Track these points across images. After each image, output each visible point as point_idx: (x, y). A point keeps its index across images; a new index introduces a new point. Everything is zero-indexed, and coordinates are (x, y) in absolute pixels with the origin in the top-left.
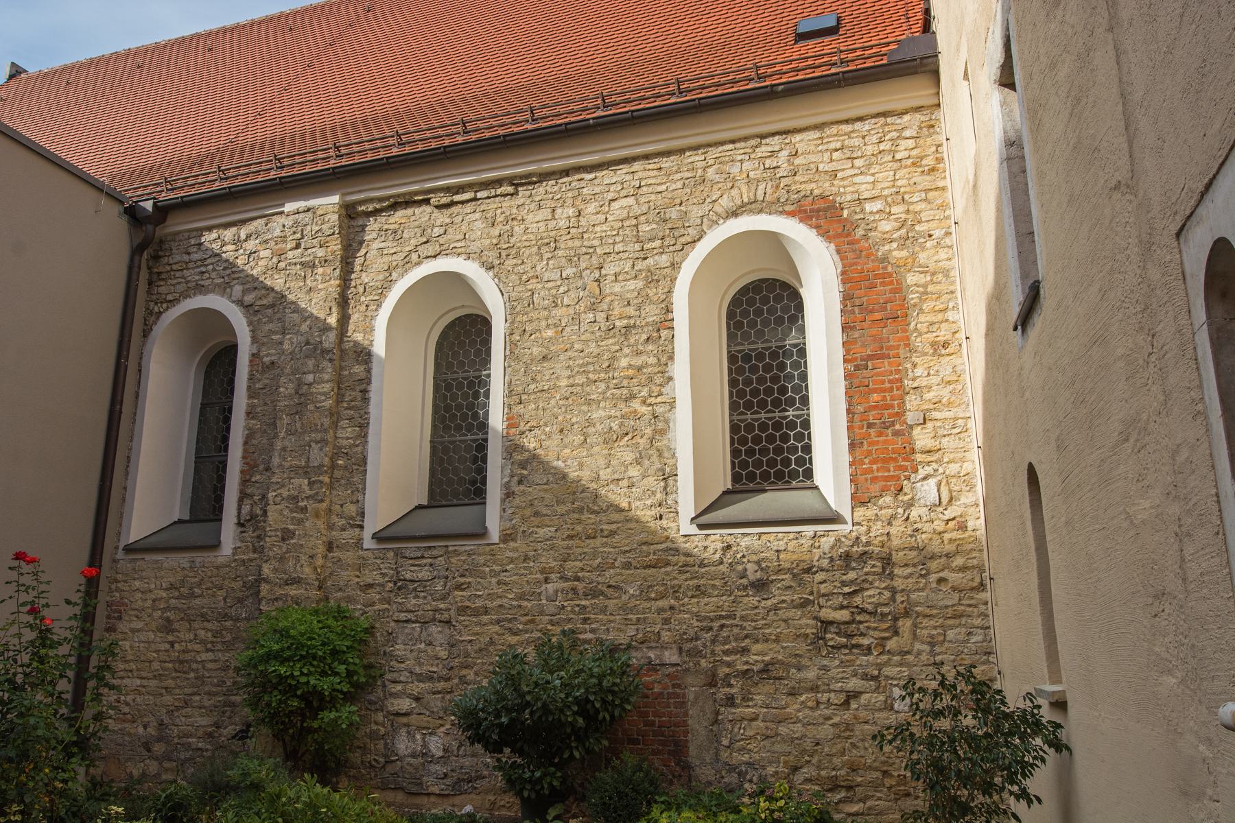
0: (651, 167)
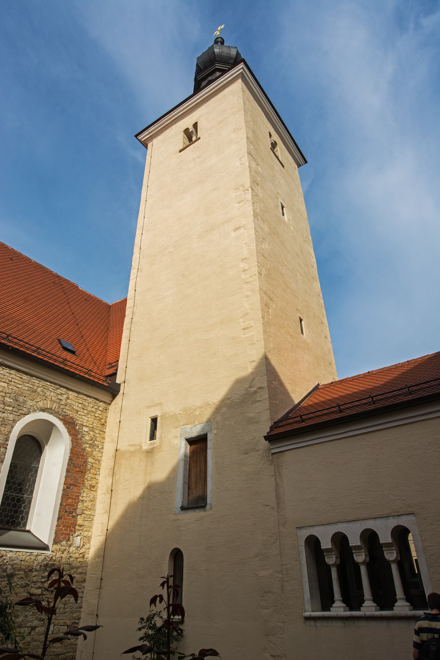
0: (18, 375)
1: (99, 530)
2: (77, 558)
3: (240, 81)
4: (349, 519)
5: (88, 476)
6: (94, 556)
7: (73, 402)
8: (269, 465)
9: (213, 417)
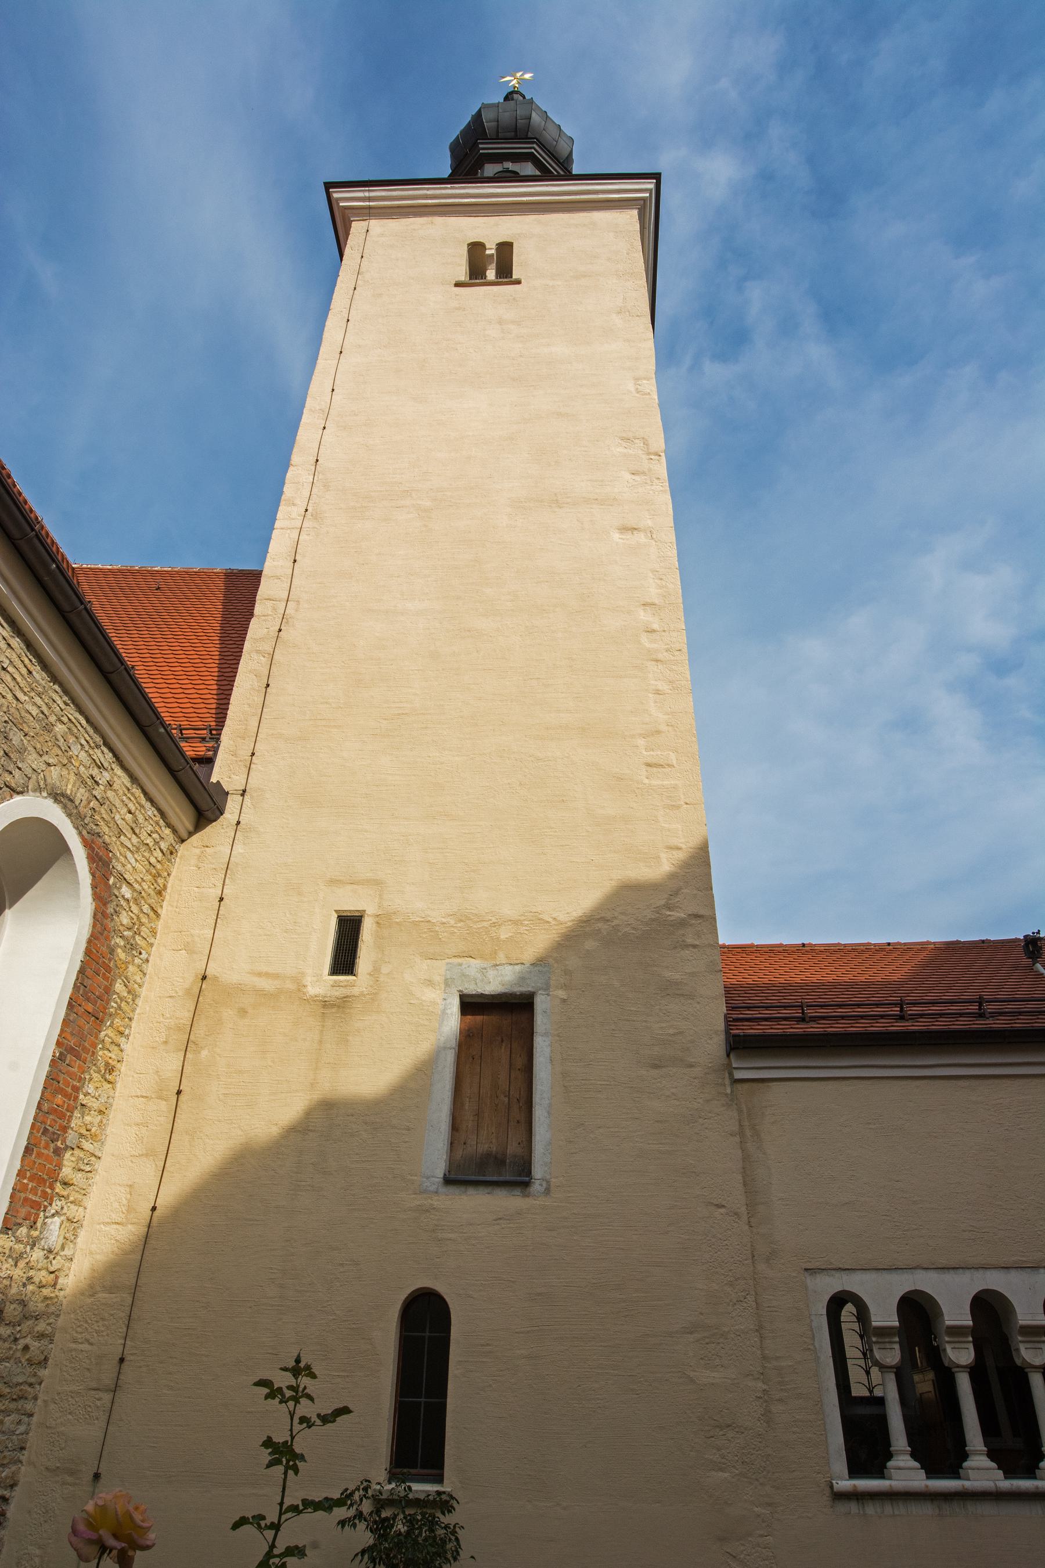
0: (27, 661)
1: (116, 1205)
2: (41, 1286)
4: (943, 1262)
5: (107, 1033)
6: (91, 1286)
7: (118, 803)
8: (723, 1105)
9: (555, 955)
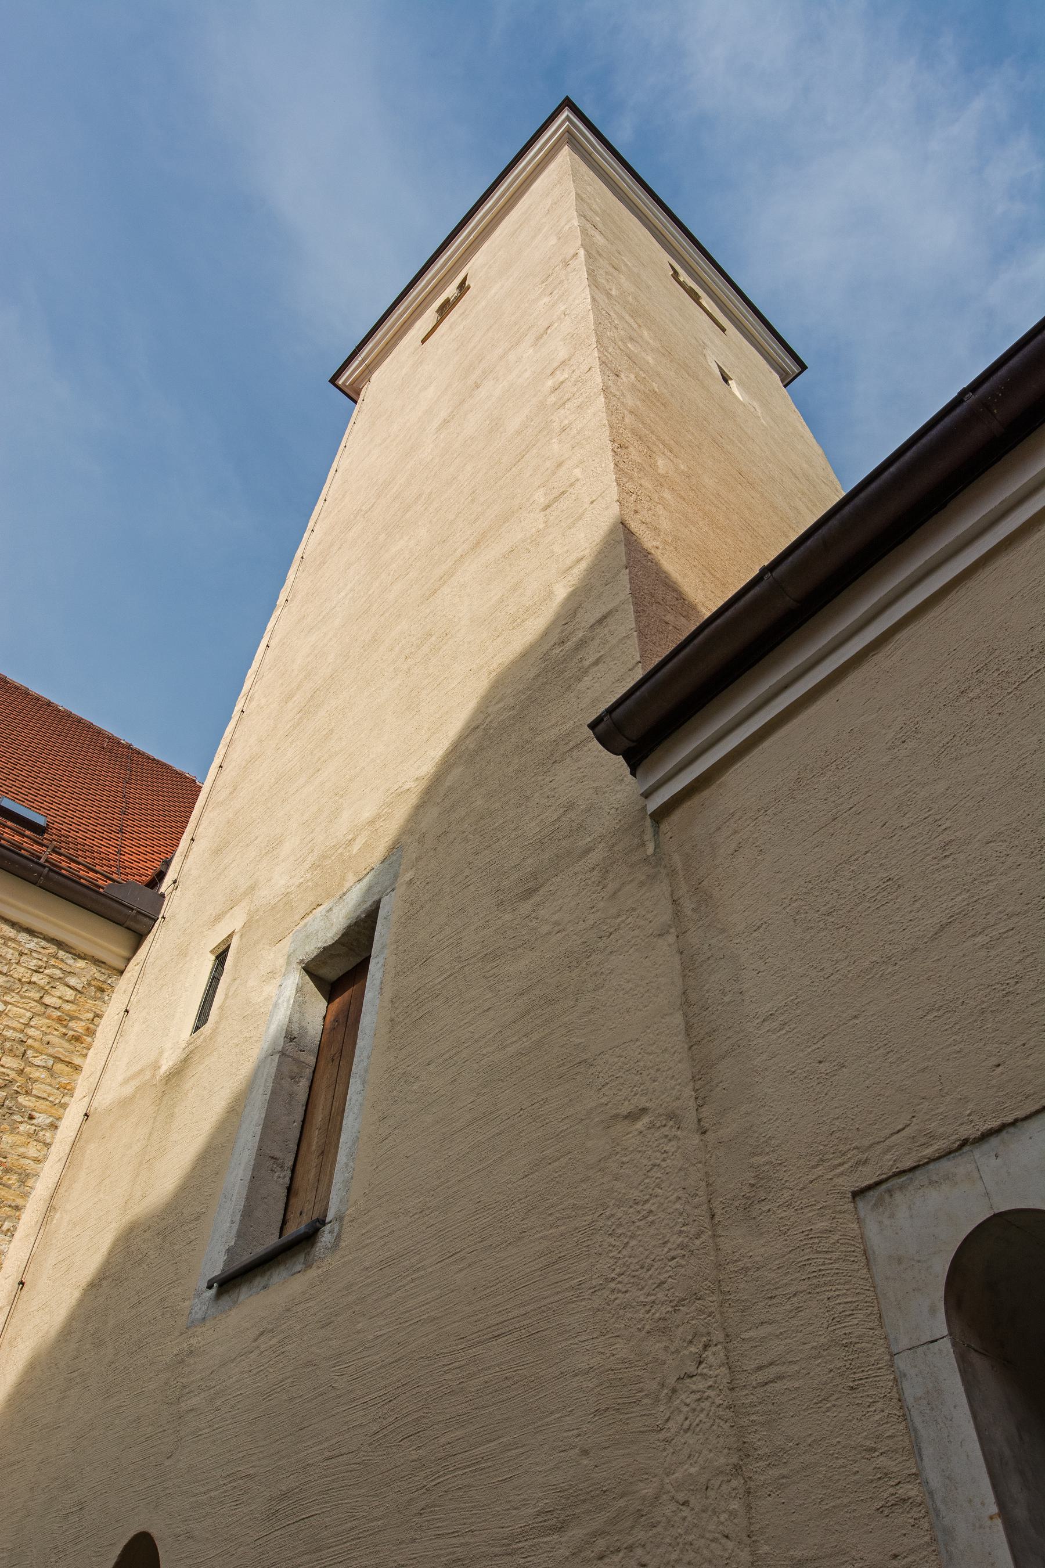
3: (566, 149)
